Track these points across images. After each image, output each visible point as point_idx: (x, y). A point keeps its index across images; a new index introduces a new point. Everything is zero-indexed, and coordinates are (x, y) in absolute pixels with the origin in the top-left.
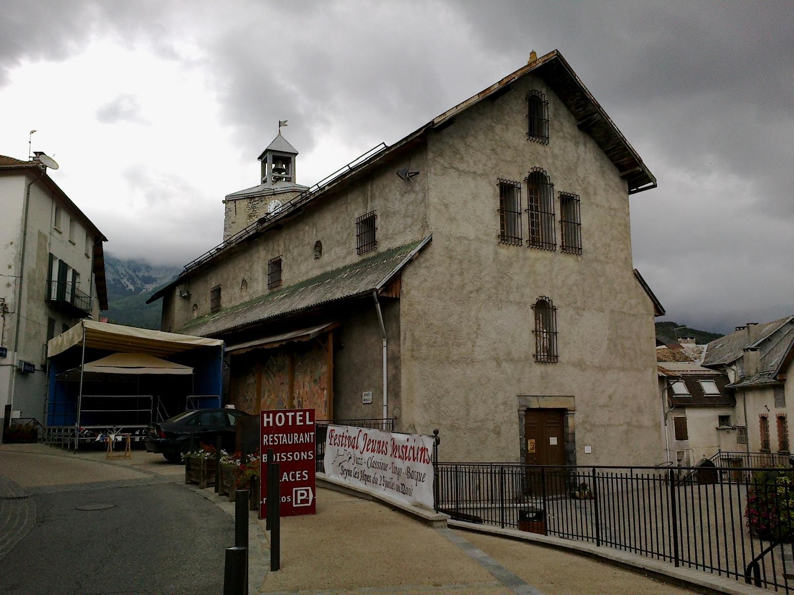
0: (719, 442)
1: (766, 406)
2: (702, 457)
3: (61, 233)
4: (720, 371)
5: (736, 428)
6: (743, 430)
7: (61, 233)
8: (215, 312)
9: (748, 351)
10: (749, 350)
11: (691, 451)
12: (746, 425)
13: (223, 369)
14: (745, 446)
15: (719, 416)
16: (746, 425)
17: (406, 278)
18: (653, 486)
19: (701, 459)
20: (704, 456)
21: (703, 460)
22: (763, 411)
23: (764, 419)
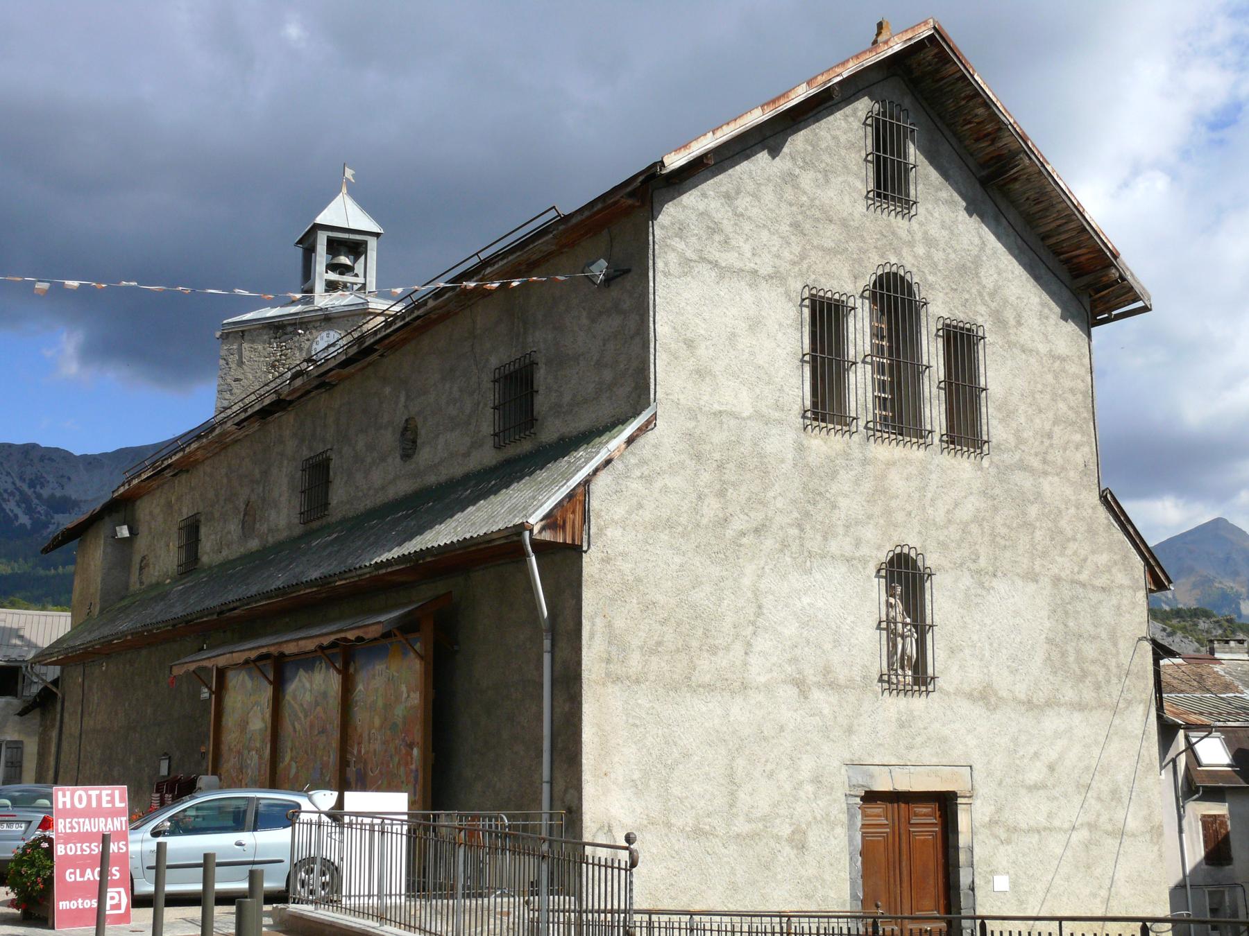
11: (1239, 890)
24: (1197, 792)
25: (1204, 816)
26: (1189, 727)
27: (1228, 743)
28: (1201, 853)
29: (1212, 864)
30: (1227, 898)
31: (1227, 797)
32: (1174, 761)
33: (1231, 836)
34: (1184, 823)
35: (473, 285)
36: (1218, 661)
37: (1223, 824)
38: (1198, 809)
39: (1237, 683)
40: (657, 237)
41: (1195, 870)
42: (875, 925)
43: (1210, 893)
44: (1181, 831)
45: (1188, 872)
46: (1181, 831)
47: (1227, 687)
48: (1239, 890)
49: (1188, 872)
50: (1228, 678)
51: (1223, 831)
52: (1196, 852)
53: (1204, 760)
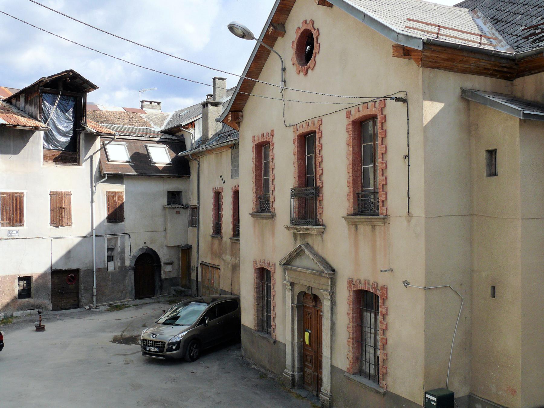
0: (165, 224)
1: (221, 176)
2: (143, 245)
3: (494, 297)
4: (176, 136)
5: (187, 208)
6: (195, 210)
7: (494, 297)
8: (267, 294)
9: (207, 106)
10: (209, 105)
11: (127, 237)
12: (199, 203)
13: (188, 357)
14: (196, 229)
15: (169, 192)
16: (199, 203)
17: (195, 123)
18: (329, 356)
19: (141, 247)
20: (145, 243)
21: (143, 248)
22: (218, 184)
23: (218, 195)
24: (104, 177)
25: (109, 192)
26: (104, 135)
27: (129, 148)
28: (104, 215)
29: (112, 222)
30: (119, 242)
31: (125, 181)
32: (91, 157)
33: (125, 204)
34: (95, 196)
35: (180, 154)
36: (145, 113)
37: (120, 197)
38: (105, 188)
39: (150, 122)
40: (495, 402)
41: (100, 225)
42: (372, 193)
43: (108, 240)
44: (92, 201)
45: (94, 227)
46: (92, 201)
47: (144, 124)
48: (127, 237)
49: (94, 227)
50: (147, 120)
51: (120, 202)
52: (101, 214)
53: (111, 158)
